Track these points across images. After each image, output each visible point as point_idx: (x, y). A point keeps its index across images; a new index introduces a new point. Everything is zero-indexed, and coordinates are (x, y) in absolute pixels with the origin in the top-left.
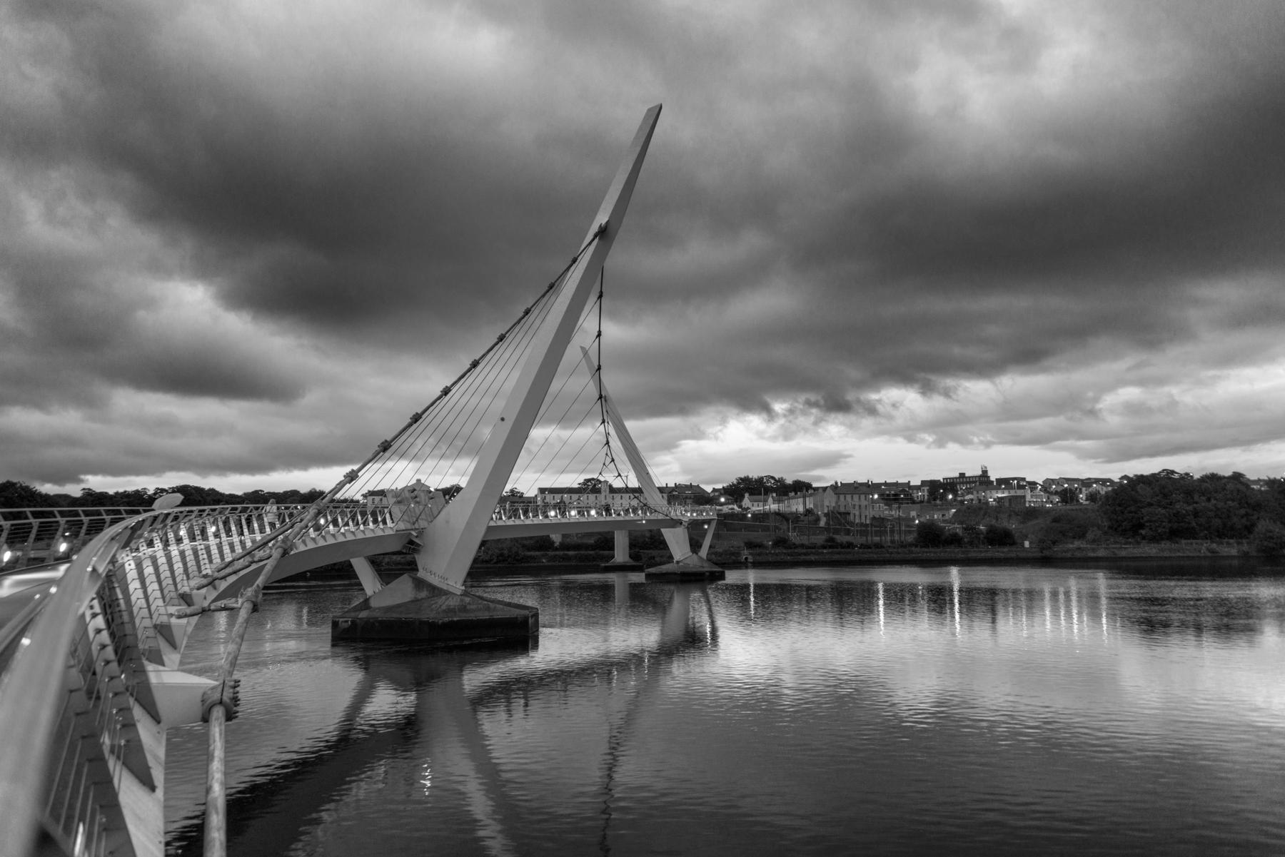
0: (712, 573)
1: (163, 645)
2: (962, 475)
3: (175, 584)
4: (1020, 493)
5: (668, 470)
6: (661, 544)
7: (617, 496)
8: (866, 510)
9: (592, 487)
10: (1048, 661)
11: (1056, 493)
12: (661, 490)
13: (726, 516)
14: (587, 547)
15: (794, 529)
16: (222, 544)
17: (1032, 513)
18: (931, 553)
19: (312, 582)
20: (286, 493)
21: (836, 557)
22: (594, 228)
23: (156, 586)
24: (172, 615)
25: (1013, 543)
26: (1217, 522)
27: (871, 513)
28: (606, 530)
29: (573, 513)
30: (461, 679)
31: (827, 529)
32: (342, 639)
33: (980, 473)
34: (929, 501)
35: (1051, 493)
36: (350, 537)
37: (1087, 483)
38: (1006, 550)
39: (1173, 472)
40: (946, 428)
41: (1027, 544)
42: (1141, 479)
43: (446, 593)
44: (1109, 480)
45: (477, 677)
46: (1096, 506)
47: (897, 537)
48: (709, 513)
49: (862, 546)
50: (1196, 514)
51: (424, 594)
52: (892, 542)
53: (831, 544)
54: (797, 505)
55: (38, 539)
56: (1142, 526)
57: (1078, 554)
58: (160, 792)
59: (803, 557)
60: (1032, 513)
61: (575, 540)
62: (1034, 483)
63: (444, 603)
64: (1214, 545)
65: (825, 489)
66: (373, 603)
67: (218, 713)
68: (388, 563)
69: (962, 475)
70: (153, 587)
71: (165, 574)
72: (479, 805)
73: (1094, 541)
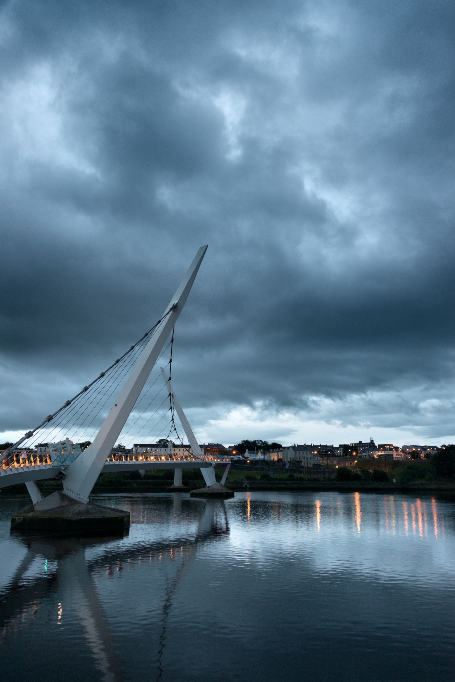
2: (360, 442)
4: (390, 452)
5: (203, 437)
7: (177, 449)
9: (163, 444)
11: (409, 453)
12: (201, 446)
13: (236, 462)
15: (272, 469)
17: (397, 463)
22: (170, 306)
27: (312, 462)
29: (152, 458)
31: (289, 470)
34: (343, 456)
37: (424, 448)
38: (383, 483)
41: (394, 481)
47: (326, 475)
51: (65, 503)
52: (324, 478)
53: (292, 478)
54: (274, 457)
66: (37, 508)
68: (47, 485)
69: (360, 442)
72: (92, 634)
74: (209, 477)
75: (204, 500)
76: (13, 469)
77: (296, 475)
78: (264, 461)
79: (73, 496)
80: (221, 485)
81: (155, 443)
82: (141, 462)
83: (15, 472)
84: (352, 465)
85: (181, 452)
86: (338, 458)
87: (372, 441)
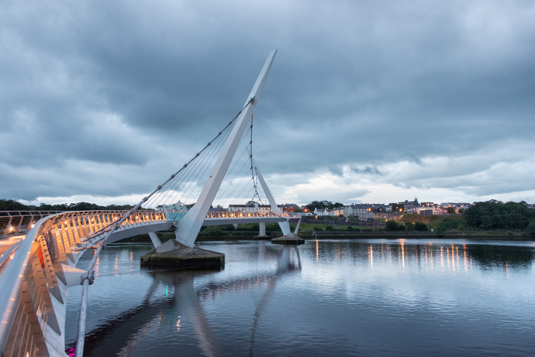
0: (299, 241)
1: (69, 261)
2: (407, 201)
3: (75, 240)
4: (430, 209)
5: (281, 200)
6: (278, 228)
7: (262, 208)
8: (365, 215)
9: (251, 205)
10: (444, 280)
11: (446, 209)
12: (279, 206)
13: (307, 217)
14: (248, 230)
15: (335, 223)
16: (94, 224)
17: (435, 217)
18: (392, 233)
19: (134, 241)
20: (124, 206)
21: (352, 235)
22: (249, 99)
23: (68, 242)
24: (72, 250)
25: (426, 230)
26: (513, 222)
27: (367, 217)
28: (255, 222)
29: (241, 215)
30: (192, 282)
31: (349, 223)
32: (145, 265)
33: (414, 200)
34: (392, 212)
35: (444, 209)
36: (148, 224)
37: (458, 205)
38: (423, 232)
39: (496, 201)
40: (411, 181)
41: (432, 230)
42: (481, 204)
43: (187, 247)
44: (469, 204)
45: (200, 281)
46: (462, 215)
47: (378, 227)
48: (299, 216)
49: (363, 230)
50: (504, 218)
51: (178, 247)
52: (376, 229)
53: (350, 229)
54: (336, 213)
55: (22, 224)
56: (481, 223)
57: (454, 235)
58: (65, 305)
59: (338, 235)
60: (435, 217)
61: (243, 226)
62: (437, 205)
63: (186, 251)
64: (511, 232)
65: (348, 206)
66: (157, 251)
67: (86, 282)
68: (166, 235)
69: (407, 201)
70: (66, 243)
71: (71, 236)
72: (201, 336)
73: (461, 229)
74: (285, 228)
75: (282, 246)
76: (138, 224)
77: (354, 227)
78: (329, 217)
79: (182, 242)
80: (295, 235)
81: (245, 204)
82: (233, 218)
83: (139, 225)
84: (399, 219)
85: (263, 211)
86: (387, 214)
87: (416, 200)
